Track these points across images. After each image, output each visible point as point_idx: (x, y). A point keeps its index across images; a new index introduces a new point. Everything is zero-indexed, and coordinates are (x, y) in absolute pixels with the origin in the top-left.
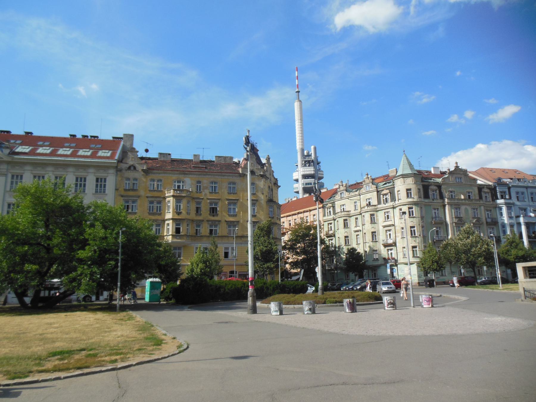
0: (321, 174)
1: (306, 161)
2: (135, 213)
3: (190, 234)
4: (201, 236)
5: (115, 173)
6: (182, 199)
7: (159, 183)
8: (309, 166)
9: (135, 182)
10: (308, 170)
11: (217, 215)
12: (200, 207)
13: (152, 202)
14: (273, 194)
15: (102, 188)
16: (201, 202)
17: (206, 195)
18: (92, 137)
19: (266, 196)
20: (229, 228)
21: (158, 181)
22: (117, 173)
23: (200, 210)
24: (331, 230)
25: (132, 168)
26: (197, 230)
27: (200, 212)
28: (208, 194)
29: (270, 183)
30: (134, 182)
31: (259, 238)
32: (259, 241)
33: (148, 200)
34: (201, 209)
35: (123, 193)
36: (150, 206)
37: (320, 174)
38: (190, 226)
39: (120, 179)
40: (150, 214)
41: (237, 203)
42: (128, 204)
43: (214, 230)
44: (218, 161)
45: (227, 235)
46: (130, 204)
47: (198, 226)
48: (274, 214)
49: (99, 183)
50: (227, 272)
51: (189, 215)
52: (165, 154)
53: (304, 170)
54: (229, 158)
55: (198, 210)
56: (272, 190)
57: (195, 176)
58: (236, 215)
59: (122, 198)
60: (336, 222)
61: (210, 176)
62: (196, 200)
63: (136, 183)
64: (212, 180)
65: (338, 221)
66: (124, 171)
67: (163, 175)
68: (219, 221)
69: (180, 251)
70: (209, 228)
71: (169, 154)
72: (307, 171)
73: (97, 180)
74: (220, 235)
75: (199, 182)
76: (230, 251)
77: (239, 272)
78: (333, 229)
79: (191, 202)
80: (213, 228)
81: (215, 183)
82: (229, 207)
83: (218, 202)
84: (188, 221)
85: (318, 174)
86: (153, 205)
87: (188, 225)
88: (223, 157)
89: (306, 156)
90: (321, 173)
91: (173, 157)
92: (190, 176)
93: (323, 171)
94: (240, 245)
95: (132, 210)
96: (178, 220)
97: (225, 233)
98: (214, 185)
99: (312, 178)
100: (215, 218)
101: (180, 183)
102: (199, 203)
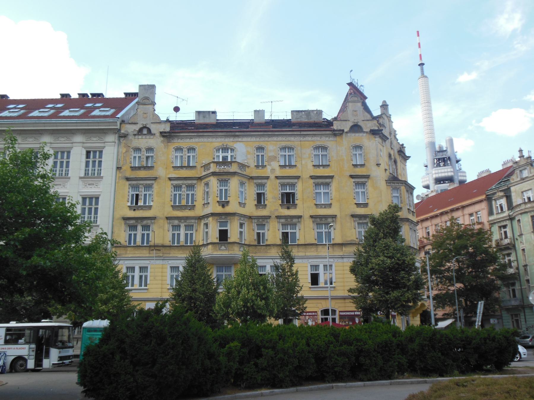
0: (463, 176)
1: (439, 159)
2: (150, 207)
3: (247, 243)
4: (267, 245)
5: (117, 141)
6: (229, 179)
7: (191, 154)
8: (444, 165)
9: (150, 155)
10: (443, 171)
11: (295, 206)
12: (264, 194)
13: (177, 187)
14: (397, 169)
15: (97, 168)
16: (266, 183)
17: (273, 170)
18: (92, 94)
19: (386, 170)
20: (318, 229)
21: (188, 150)
22: (119, 140)
23: (264, 198)
24: (506, 237)
25: (145, 131)
26: (258, 234)
27: (264, 203)
28: (277, 169)
29: (392, 149)
30: (148, 155)
31: (375, 241)
32: (376, 246)
33: (172, 184)
34: (265, 196)
35: (130, 174)
36: (175, 195)
37: (461, 176)
38: (246, 227)
39: (124, 150)
40: (174, 207)
41: (330, 182)
42: (137, 193)
43: (290, 233)
44: (297, 118)
45: (316, 242)
46: (142, 192)
47: (261, 226)
48: (401, 201)
49: (91, 160)
50: (316, 312)
51: (244, 207)
52: (206, 112)
53: (437, 172)
54: (315, 112)
55: (260, 197)
56: (395, 162)
57: (254, 139)
58: (331, 204)
59: (128, 183)
60: (515, 223)
61: (280, 138)
62: (255, 181)
63: (152, 157)
64: (284, 144)
65: (519, 221)
66: (131, 137)
67: (197, 140)
68: (300, 217)
69: (229, 273)
70: (281, 231)
71: (214, 113)
72: (441, 173)
73: (88, 153)
74: (302, 242)
75: (260, 149)
76: (321, 271)
77: (340, 312)
78: (509, 235)
79: (247, 184)
80: (289, 231)
81: (291, 148)
82: (317, 191)
83: (296, 183)
84: (242, 219)
85: (458, 176)
86: (180, 192)
87: (241, 225)
88: (304, 111)
89: (439, 152)
90: (462, 174)
91: (221, 116)
92: (245, 139)
93: (464, 172)
94: (340, 260)
95: (145, 202)
96: (223, 217)
97: (311, 238)
98: (287, 154)
99: (449, 181)
100: (292, 212)
101: (228, 152)
102: (262, 186)
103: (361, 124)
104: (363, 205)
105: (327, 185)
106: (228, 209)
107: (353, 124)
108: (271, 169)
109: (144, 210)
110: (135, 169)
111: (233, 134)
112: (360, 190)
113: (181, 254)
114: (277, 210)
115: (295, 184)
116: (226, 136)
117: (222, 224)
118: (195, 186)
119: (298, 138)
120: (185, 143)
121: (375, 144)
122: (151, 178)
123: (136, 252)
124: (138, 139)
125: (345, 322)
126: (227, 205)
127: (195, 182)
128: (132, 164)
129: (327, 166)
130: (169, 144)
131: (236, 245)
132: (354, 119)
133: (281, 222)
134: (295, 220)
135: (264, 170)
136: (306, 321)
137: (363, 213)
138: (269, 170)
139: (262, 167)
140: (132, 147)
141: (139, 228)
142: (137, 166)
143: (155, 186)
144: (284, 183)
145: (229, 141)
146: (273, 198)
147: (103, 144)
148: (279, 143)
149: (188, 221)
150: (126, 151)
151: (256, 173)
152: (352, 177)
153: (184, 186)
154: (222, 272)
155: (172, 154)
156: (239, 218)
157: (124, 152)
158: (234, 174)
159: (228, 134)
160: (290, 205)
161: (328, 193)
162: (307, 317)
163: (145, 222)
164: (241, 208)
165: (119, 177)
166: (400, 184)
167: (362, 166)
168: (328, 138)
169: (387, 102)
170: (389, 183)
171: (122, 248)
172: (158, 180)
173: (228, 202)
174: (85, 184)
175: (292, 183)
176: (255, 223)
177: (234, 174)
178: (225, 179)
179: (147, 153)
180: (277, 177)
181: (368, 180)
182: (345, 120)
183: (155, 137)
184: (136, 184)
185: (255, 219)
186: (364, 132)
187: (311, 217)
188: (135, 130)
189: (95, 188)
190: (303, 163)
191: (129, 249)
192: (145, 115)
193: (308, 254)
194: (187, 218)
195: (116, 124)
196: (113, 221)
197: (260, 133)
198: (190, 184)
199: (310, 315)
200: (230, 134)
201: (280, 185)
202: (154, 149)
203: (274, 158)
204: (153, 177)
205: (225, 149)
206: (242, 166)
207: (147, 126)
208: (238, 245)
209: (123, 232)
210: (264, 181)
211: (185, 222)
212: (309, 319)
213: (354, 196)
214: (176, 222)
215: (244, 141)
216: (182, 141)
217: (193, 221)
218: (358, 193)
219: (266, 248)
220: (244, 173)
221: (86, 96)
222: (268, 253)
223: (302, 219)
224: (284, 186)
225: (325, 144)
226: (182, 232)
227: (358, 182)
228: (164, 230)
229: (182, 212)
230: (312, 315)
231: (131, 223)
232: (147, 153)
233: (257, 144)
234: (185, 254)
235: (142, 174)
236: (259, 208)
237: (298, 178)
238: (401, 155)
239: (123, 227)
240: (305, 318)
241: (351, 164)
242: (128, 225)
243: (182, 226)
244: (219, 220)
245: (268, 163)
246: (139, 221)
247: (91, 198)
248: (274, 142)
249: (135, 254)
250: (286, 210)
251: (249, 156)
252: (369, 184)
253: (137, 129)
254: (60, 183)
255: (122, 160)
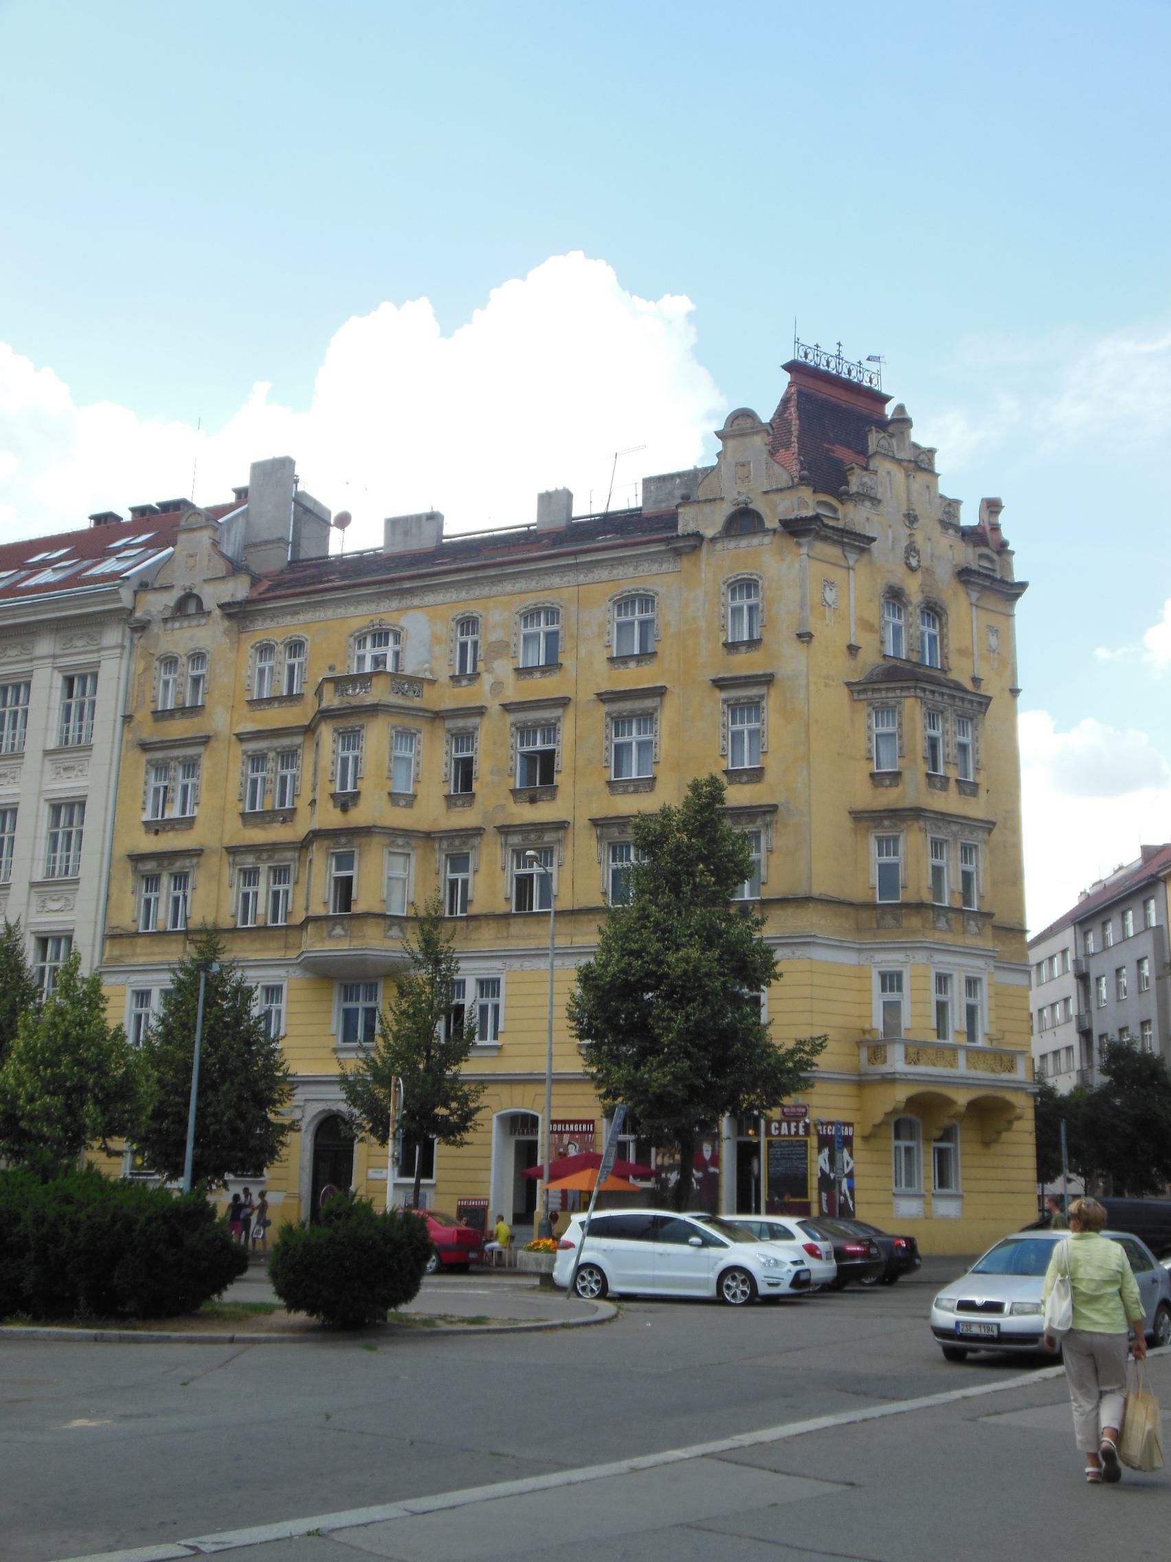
2: (189, 823)
5: (127, 643)
6: (362, 727)
13: (257, 760)
16: (476, 728)
17: (498, 686)
35: (149, 731)
41: (655, 709)
50: (592, 1122)
55: (465, 772)
57: (452, 595)
58: (654, 779)
59: (144, 757)
61: (521, 585)
62: (450, 724)
64: (530, 600)
66: (156, 628)
67: (308, 616)
68: (562, 826)
73: (69, 681)
84: (400, 841)
92: (429, 599)
96: (343, 840)
100: (544, 812)
103: (759, 505)
104: (748, 775)
105: (647, 718)
106: (359, 816)
107: (736, 508)
108: (492, 681)
109: (177, 830)
110: (163, 716)
111: (397, 587)
112: (746, 727)
113: (257, 951)
114: (502, 807)
115: (555, 724)
116: (381, 596)
117: (345, 861)
118: (300, 751)
119: (571, 578)
120: (275, 630)
121: (797, 566)
122: (196, 738)
123: (156, 950)
124: (173, 630)
125: (672, 1156)
126: (355, 805)
127: (298, 740)
128: (521, 659)
129: (647, 657)
130: (243, 636)
131: (371, 920)
132: (739, 492)
133: (512, 845)
134: (548, 837)
135: (475, 687)
136: (561, 1150)
137: (746, 803)
138: (487, 687)
139: (470, 680)
140: (157, 656)
141: (165, 881)
142: (187, 705)
143: (205, 762)
144: (525, 722)
145: (386, 612)
146: (492, 773)
147: (96, 655)
148: (517, 599)
149: (277, 856)
150: (146, 669)
151: (446, 698)
152: (719, 684)
153: (272, 755)
154: (357, 1000)
155: (250, 663)
156: (387, 841)
157: (140, 670)
158: (374, 710)
159: (385, 588)
160: (538, 791)
161: (408, 760)
162: (566, 1138)
163: (178, 865)
164: (397, 810)
165: (127, 742)
166: (898, 693)
167: (183, 711)
168: (656, 566)
169: (908, 409)
170: (859, 692)
171: (124, 940)
172: (212, 744)
173: (356, 796)
174: (57, 768)
175: (545, 719)
176: (444, 850)
177: (374, 710)
178: (352, 727)
179: (619, 615)
180: (507, 708)
181: (768, 689)
182: (710, 501)
183: (211, 622)
184: (163, 759)
185: (441, 839)
186: (765, 531)
187: (595, 823)
188: (166, 607)
189: (10, 786)
190: (583, 653)
191: (140, 941)
192: (191, 561)
193: (514, 944)
194: (273, 848)
195: (117, 596)
196: (110, 866)
197: (464, 576)
198: (287, 746)
199: (574, 1132)
200: (389, 587)
201: (513, 729)
202: (208, 656)
203: (502, 648)
204: (202, 734)
205: (381, 636)
206: (416, 683)
207: (195, 591)
208: (382, 922)
209: (129, 895)
210: (470, 722)
211: (270, 858)
212: (569, 1143)
213: (723, 749)
214: (249, 861)
215: (427, 604)
216: (273, 625)
217: (289, 855)
218: (737, 737)
219: (467, 927)
220: (417, 702)
221: (182, 506)
222: (475, 940)
223: (570, 831)
224: (623, 722)
225: (648, 587)
226: (263, 887)
227: (738, 699)
228: (219, 884)
229: (264, 829)
230: (578, 1132)
231: (147, 870)
232: (525, 626)
233: (459, 611)
234: (179, 953)
235: (178, 729)
236: (456, 805)
237: (563, 702)
238: (974, 583)
239: (130, 881)
240: (561, 1140)
241: (720, 644)
242: (143, 877)
243: (264, 868)
244: (332, 851)
245: (485, 664)
246: (166, 862)
247: (71, 806)
248: (507, 598)
249: (153, 954)
250: (528, 804)
251: (437, 649)
252: (771, 704)
253: (172, 604)
254: (5, 771)
255: (136, 694)
